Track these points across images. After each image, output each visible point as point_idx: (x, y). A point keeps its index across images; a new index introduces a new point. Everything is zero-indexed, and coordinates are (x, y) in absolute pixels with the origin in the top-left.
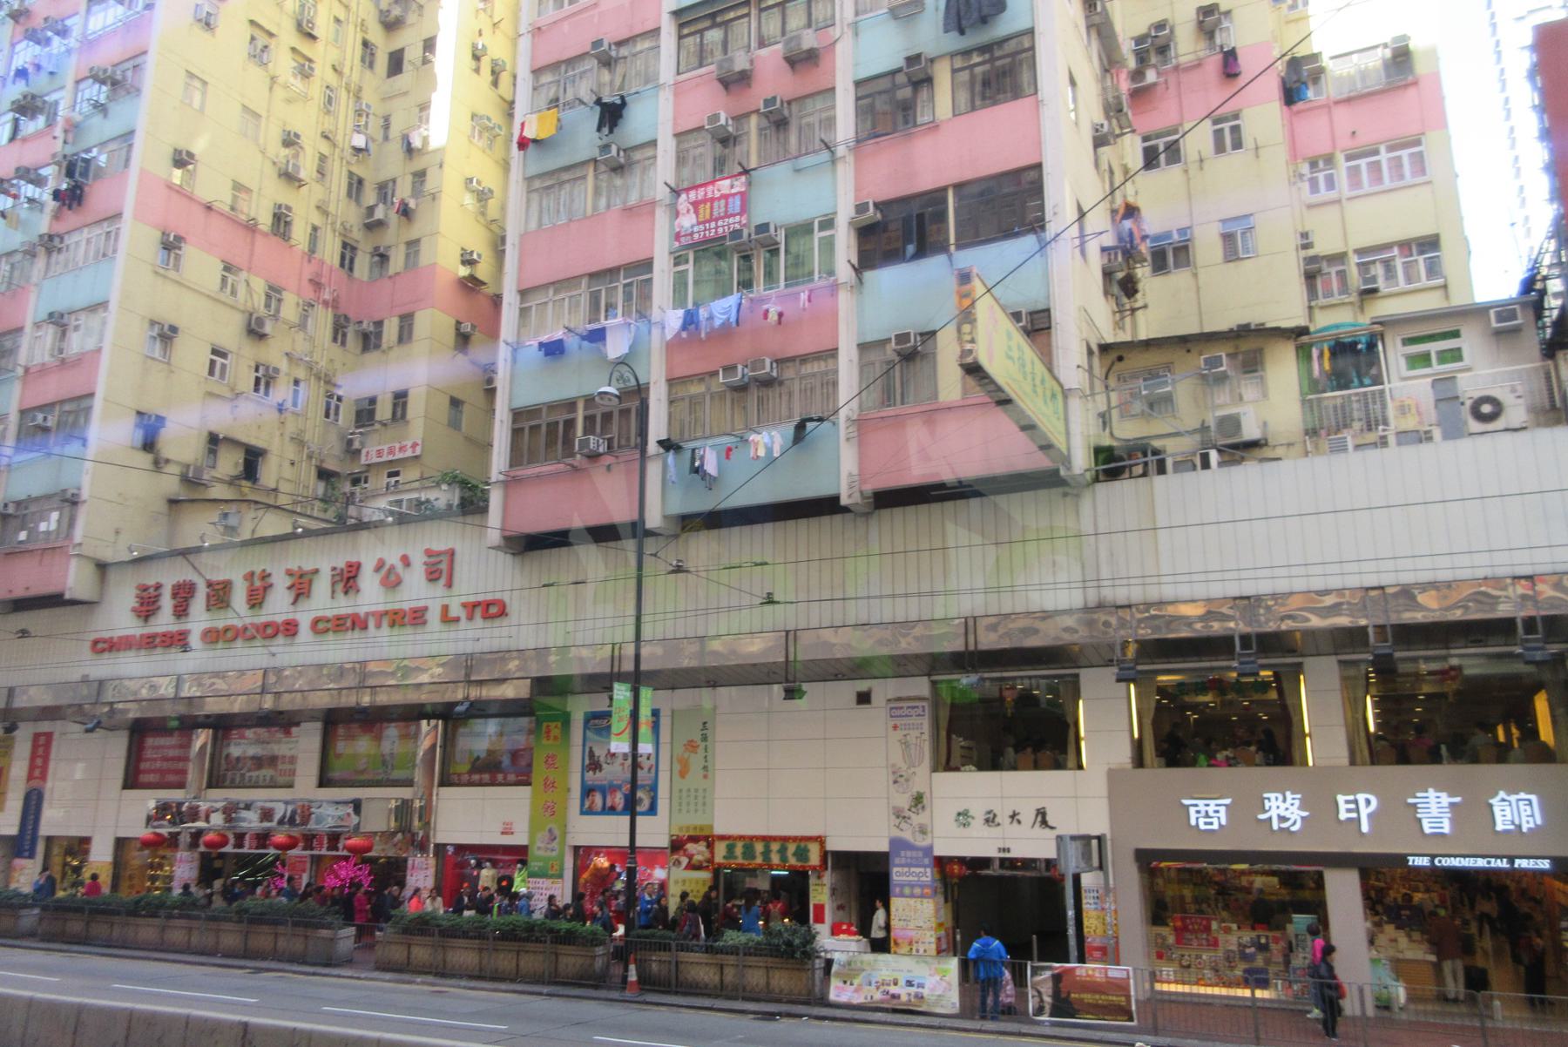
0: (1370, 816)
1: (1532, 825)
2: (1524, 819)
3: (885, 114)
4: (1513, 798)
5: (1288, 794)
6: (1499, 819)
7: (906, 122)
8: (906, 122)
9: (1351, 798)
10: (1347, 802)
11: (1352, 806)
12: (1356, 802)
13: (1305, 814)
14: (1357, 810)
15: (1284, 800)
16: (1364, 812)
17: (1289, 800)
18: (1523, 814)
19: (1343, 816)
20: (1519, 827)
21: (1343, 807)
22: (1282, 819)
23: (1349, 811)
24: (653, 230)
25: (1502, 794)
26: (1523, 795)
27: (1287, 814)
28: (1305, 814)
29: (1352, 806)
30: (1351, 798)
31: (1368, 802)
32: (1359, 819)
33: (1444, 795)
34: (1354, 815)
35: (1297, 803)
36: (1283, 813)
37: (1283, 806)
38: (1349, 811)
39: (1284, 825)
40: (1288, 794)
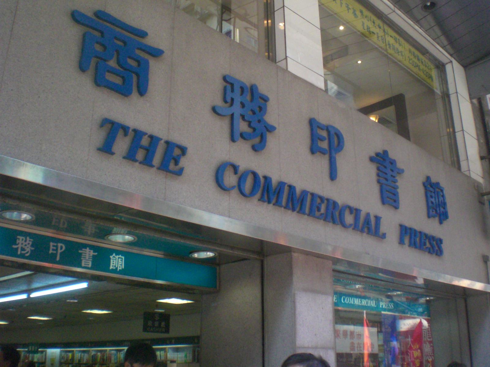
0: (61, 253)
1: (121, 268)
2: (119, 266)
3: (163, 327)
4: (117, 257)
5: (28, 238)
6: (112, 264)
7: (88, 360)
8: (88, 360)
9: (55, 244)
10: (54, 246)
11: (55, 248)
12: (57, 246)
13: (33, 249)
14: (57, 250)
15: (26, 241)
16: (59, 251)
17: (28, 242)
18: (119, 264)
19: (51, 252)
20: (117, 268)
21: (51, 247)
22: (23, 249)
23: (53, 250)
24: (431, 38)
25: (114, 255)
26: (120, 256)
27: (26, 247)
28: (33, 249)
29: (55, 248)
30: (55, 244)
31: (61, 248)
32: (57, 254)
33: (92, 251)
34: (55, 252)
35: (31, 243)
36: (24, 247)
37: (24, 244)
38: (53, 250)
39: (23, 252)
40: (28, 238)
